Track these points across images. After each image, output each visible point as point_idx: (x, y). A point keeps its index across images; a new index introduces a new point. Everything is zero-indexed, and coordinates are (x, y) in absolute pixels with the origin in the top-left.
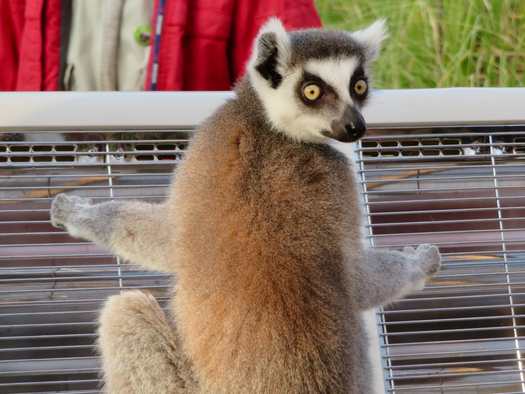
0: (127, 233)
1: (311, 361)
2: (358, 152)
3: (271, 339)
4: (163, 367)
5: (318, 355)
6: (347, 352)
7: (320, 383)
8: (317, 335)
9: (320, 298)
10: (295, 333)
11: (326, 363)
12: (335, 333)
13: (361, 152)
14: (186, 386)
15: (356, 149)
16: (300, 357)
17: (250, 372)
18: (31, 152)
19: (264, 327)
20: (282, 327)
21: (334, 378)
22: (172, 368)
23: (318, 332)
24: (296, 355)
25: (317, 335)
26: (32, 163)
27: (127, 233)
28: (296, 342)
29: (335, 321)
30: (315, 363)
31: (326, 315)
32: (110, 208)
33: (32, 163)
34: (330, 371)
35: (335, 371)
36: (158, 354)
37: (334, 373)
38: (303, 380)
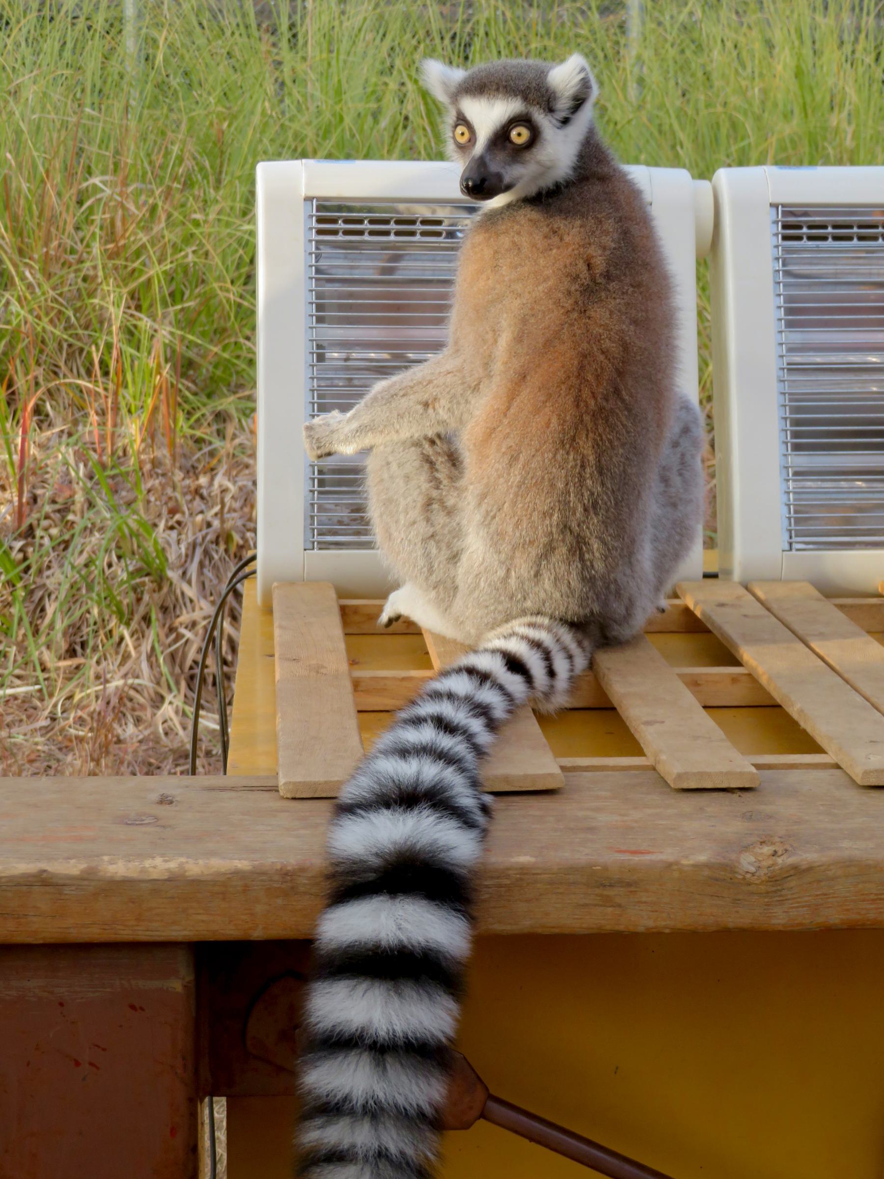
0: (394, 794)
1: (583, 467)
2: (776, 235)
3: (548, 427)
4: (417, 464)
5: (593, 462)
6: (629, 471)
7: (586, 494)
8: (602, 440)
9: (623, 401)
10: (576, 429)
11: (601, 473)
12: (623, 445)
13: (780, 236)
14: (442, 487)
15: (775, 231)
16: (571, 457)
17: (514, 459)
18: (392, 226)
19: (547, 410)
20: (565, 416)
21: (607, 494)
22: (427, 466)
23: (604, 437)
24: (568, 453)
25: (602, 440)
26: (392, 238)
27: (394, 794)
28: (573, 439)
29: (628, 432)
30: (588, 470)
31: (621, 422)
32: (455, 549)
33: (392, 238)
34: (603, 484)
35: (609, 486)
36: (413, 448)
37: (608, 488)
38: (567, 484)
